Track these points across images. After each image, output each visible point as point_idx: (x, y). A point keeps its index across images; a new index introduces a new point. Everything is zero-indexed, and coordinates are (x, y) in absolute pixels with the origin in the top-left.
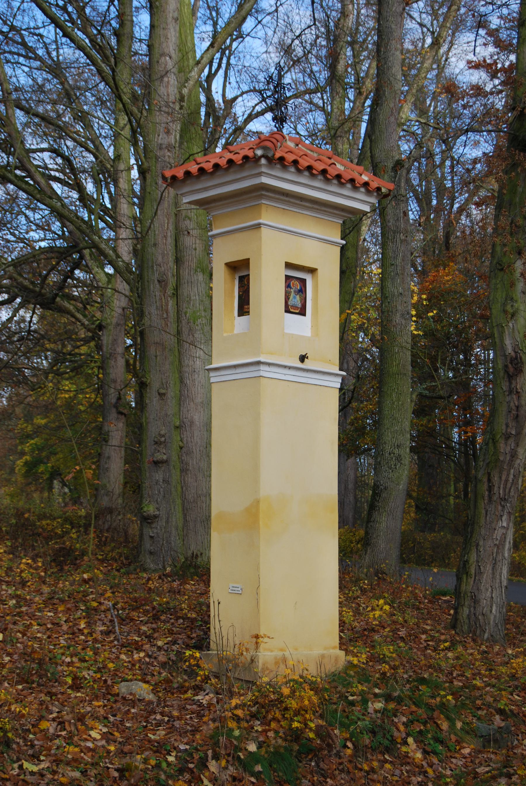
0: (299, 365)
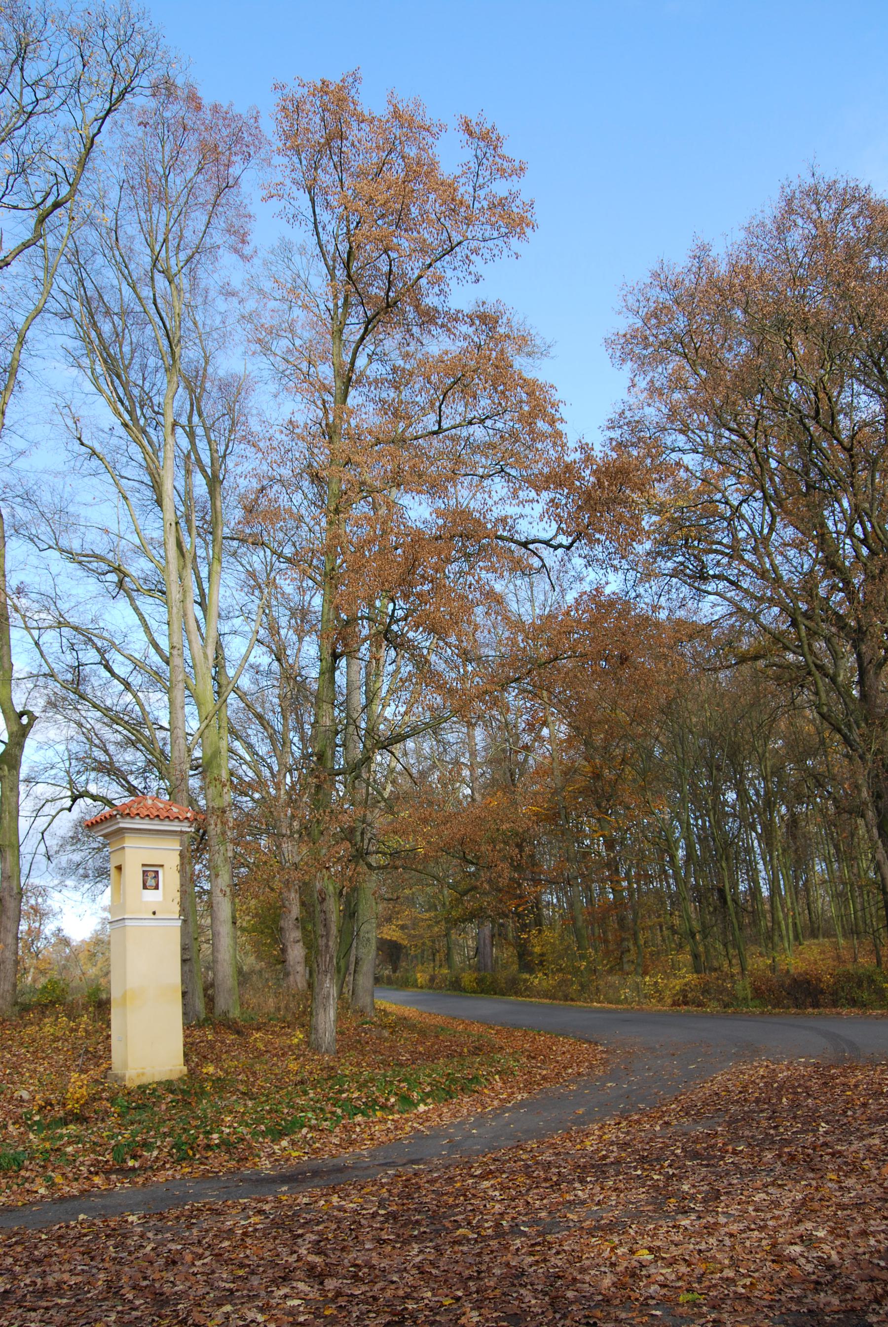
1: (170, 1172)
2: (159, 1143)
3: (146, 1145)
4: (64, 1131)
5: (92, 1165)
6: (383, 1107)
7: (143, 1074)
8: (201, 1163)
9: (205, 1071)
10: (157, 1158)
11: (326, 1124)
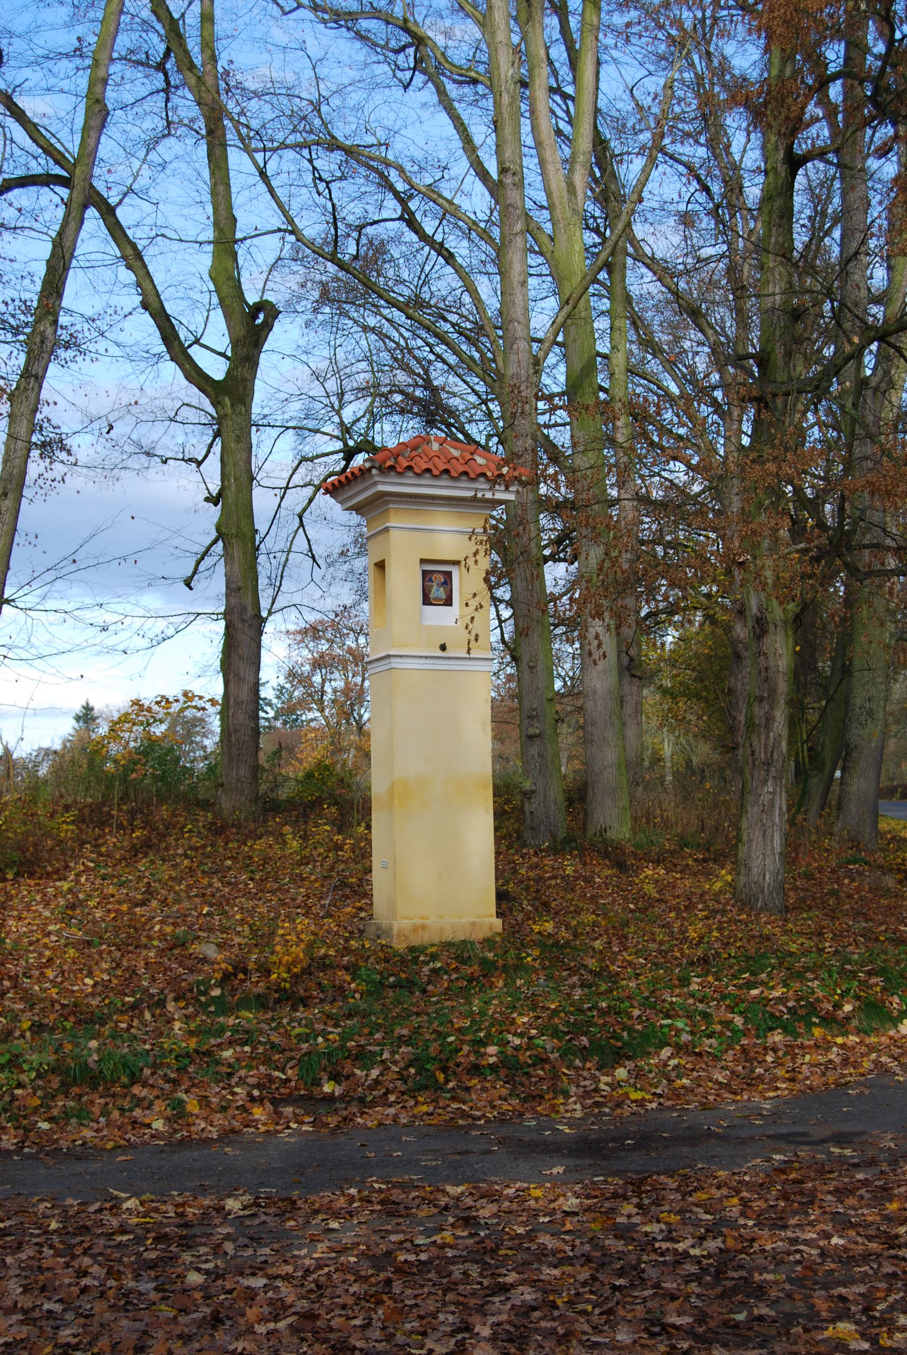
0: (441, 654)
1: (391, 1111)
2: (386, 1055)
3: (362, 1057)
4: (231, 1021)
5: (258, 1086)
6: (828, 1020)
7: (424, 927)
8: (454, 1099)
9: (536, 928)
10: (377, 1082)
11: (709, 1044)
